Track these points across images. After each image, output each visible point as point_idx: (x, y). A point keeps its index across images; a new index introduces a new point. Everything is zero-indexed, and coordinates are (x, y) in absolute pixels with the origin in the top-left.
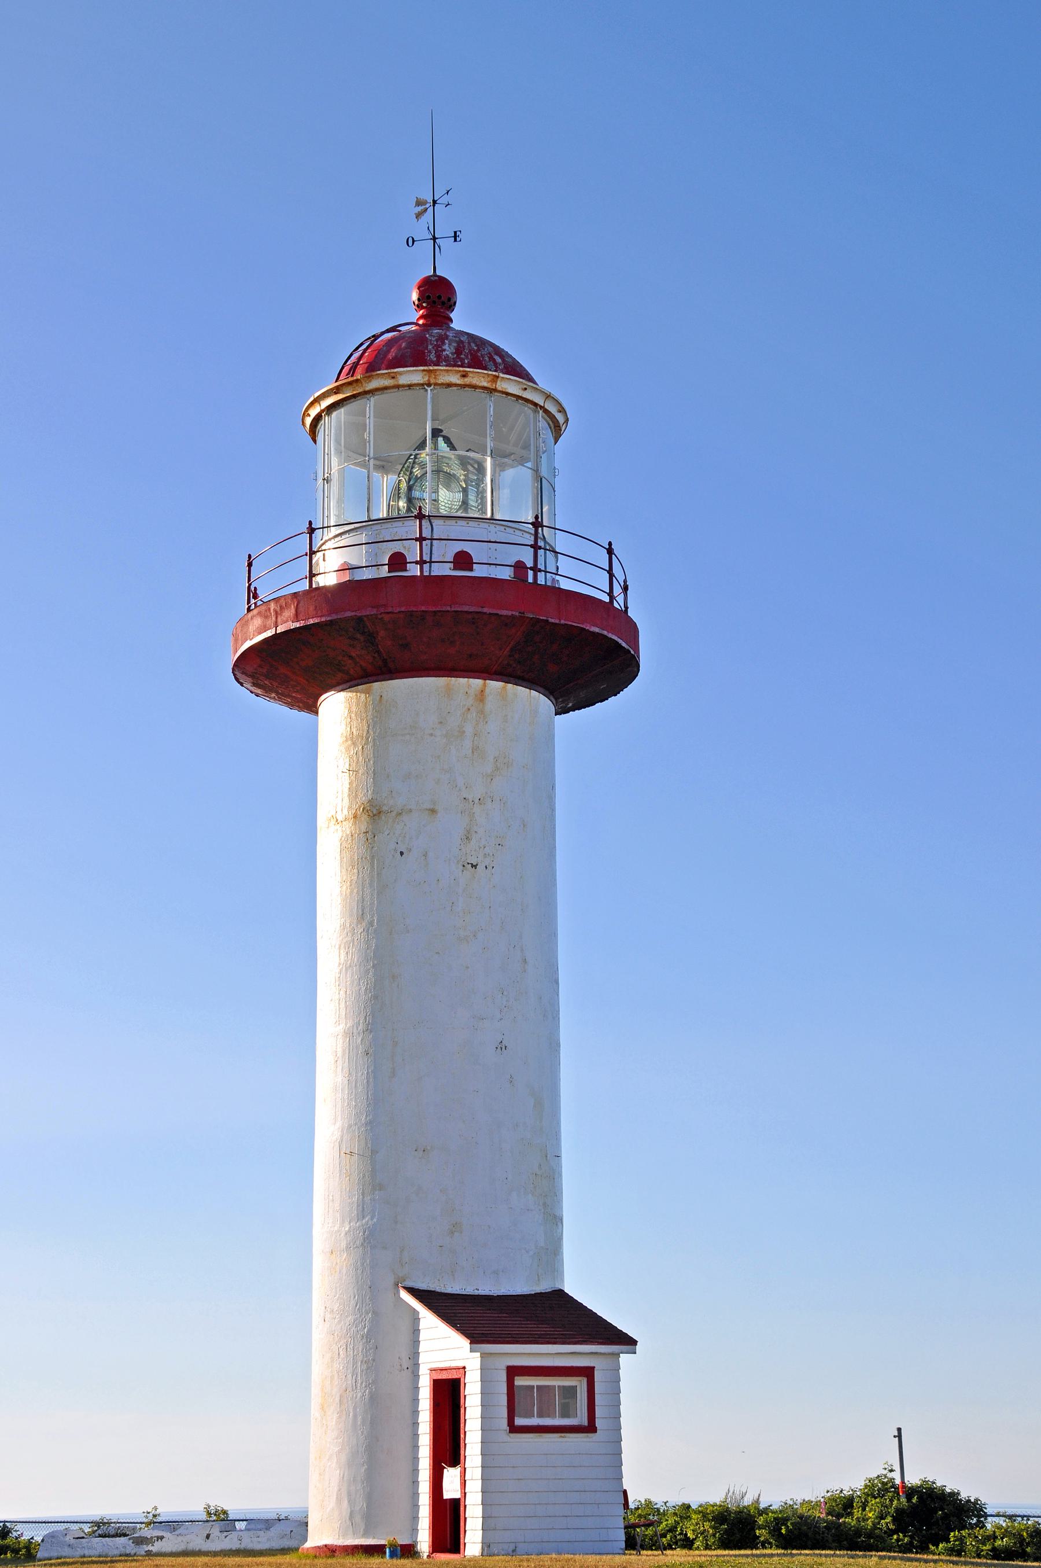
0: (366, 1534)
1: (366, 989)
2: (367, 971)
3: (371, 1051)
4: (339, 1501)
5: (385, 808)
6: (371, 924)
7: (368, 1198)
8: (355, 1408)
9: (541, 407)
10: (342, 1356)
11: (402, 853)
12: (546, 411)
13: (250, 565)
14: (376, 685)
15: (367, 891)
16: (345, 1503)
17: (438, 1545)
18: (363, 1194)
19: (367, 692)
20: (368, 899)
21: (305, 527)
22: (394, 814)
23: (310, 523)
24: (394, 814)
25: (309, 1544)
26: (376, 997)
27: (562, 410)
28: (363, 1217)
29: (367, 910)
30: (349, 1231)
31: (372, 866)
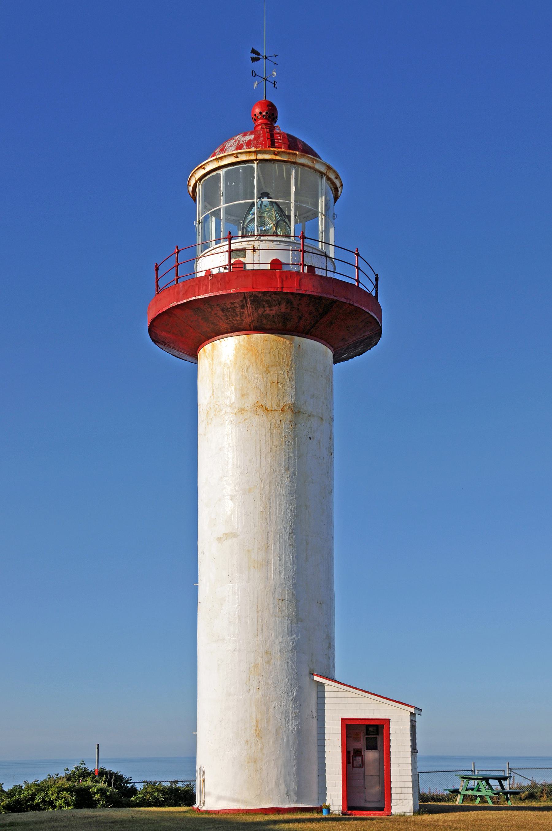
0: (297, 802)
1: (291, 510)
2: (291, 501)
3: (294, 545)
4: (277, 784)
5: (301, 410)
6: (294, 474)
7: (294, 626)
8: (287, 737)
9: (325, 175)
10: (277, 708)
11: (310, 438)
12: (329, 179)
13: (157, 269)
14: (297, 338)
15: (291, 455)
16: (283, 786)
17: (351, 806)
18: (291, 622)
19: (291, 340)
20: (292, 459)
21: (174, 250)
22: (306, 415)
23: (177, 247)
24: (306, 415)
25: (330, 687)
26: (297, 516)
27: (337, 177)
28: (292, 635)
29: (291, 465)
30: (282, 642)
31: (295, 442)
